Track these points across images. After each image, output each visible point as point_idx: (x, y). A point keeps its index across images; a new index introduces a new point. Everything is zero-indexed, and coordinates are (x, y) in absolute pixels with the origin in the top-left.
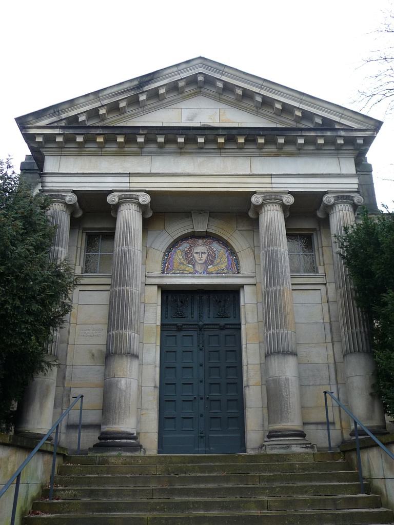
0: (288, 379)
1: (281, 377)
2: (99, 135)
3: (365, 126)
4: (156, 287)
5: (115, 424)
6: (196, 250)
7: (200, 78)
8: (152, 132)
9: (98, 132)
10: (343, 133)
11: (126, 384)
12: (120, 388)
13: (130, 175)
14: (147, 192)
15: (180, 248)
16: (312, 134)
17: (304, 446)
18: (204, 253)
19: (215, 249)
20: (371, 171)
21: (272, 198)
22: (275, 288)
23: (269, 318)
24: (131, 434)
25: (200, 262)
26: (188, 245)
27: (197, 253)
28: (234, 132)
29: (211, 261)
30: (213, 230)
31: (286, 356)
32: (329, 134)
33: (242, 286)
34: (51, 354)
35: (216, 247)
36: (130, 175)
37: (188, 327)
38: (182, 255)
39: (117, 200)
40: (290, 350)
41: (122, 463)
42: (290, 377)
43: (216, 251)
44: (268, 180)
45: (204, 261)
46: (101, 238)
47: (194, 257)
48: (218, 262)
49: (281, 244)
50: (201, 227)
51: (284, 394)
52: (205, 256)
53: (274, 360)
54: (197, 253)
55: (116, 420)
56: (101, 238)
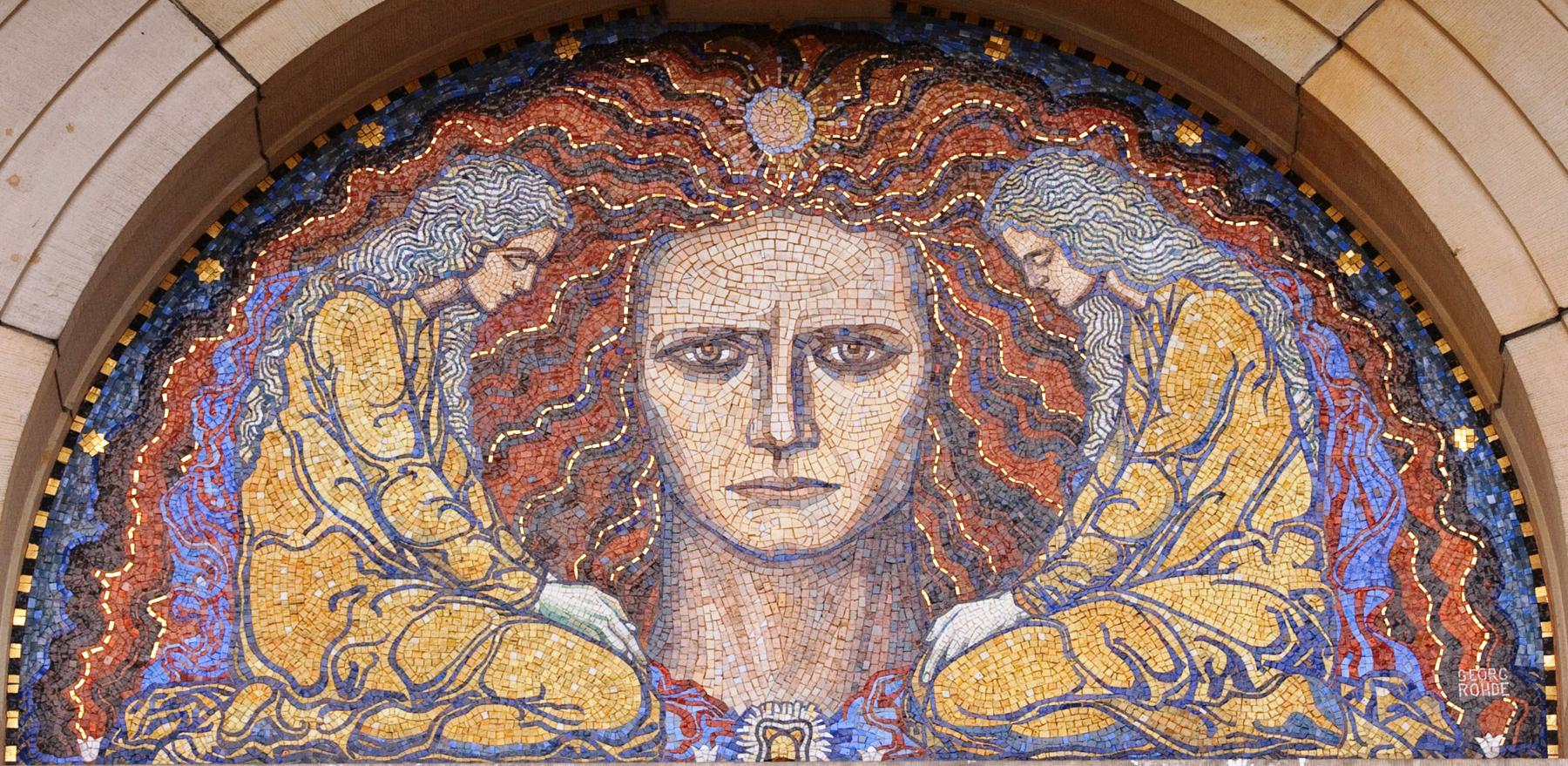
19: (1067, 281)
43: (1100, 324)
45: (846, 506)
48: (1123, 524)
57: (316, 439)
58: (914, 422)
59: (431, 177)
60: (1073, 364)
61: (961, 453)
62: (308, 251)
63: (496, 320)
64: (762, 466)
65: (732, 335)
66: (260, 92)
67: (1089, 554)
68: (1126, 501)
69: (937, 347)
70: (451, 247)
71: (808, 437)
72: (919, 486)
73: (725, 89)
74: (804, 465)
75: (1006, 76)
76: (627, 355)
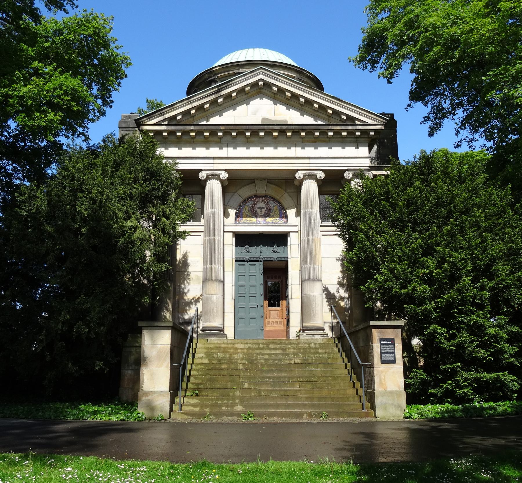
2: (192, 131)
3: (377, 122)
5: (211, 322)
6: (259, 205)
7: (261, 83)
8: (228, 128)
9: (191, 129)
10: (360, 128)
13: (214, 158)
15: (247, 204)
16: (339, 128)
17: (323, 336)
18: (264, 208)
20: (397, 126)
21: (310, 175)
23: (305, 257)
24: (220, 328)
25: (261, 214)
26: (253, 202)
27: (259, 208)
28: (284, 128)
29: (268, 214)
30: (270, 192)
31: (315, 282)
32: (350, 128)
33: (289, 232)
35: (272, 203)
36: (214, 158)
37: (253, 259)
38: (248, 210)
39: (205, 176)
40: (317, 278)
41: (73, 419)
44: (211, 161)
46: (356, 453)
47: (256, 211)
49: (315, 207)
50: (261, 191)
51: (312, 305)
52: (264, 211)
54: (259, 208)
56: (356, 453)
67: (272, 215)
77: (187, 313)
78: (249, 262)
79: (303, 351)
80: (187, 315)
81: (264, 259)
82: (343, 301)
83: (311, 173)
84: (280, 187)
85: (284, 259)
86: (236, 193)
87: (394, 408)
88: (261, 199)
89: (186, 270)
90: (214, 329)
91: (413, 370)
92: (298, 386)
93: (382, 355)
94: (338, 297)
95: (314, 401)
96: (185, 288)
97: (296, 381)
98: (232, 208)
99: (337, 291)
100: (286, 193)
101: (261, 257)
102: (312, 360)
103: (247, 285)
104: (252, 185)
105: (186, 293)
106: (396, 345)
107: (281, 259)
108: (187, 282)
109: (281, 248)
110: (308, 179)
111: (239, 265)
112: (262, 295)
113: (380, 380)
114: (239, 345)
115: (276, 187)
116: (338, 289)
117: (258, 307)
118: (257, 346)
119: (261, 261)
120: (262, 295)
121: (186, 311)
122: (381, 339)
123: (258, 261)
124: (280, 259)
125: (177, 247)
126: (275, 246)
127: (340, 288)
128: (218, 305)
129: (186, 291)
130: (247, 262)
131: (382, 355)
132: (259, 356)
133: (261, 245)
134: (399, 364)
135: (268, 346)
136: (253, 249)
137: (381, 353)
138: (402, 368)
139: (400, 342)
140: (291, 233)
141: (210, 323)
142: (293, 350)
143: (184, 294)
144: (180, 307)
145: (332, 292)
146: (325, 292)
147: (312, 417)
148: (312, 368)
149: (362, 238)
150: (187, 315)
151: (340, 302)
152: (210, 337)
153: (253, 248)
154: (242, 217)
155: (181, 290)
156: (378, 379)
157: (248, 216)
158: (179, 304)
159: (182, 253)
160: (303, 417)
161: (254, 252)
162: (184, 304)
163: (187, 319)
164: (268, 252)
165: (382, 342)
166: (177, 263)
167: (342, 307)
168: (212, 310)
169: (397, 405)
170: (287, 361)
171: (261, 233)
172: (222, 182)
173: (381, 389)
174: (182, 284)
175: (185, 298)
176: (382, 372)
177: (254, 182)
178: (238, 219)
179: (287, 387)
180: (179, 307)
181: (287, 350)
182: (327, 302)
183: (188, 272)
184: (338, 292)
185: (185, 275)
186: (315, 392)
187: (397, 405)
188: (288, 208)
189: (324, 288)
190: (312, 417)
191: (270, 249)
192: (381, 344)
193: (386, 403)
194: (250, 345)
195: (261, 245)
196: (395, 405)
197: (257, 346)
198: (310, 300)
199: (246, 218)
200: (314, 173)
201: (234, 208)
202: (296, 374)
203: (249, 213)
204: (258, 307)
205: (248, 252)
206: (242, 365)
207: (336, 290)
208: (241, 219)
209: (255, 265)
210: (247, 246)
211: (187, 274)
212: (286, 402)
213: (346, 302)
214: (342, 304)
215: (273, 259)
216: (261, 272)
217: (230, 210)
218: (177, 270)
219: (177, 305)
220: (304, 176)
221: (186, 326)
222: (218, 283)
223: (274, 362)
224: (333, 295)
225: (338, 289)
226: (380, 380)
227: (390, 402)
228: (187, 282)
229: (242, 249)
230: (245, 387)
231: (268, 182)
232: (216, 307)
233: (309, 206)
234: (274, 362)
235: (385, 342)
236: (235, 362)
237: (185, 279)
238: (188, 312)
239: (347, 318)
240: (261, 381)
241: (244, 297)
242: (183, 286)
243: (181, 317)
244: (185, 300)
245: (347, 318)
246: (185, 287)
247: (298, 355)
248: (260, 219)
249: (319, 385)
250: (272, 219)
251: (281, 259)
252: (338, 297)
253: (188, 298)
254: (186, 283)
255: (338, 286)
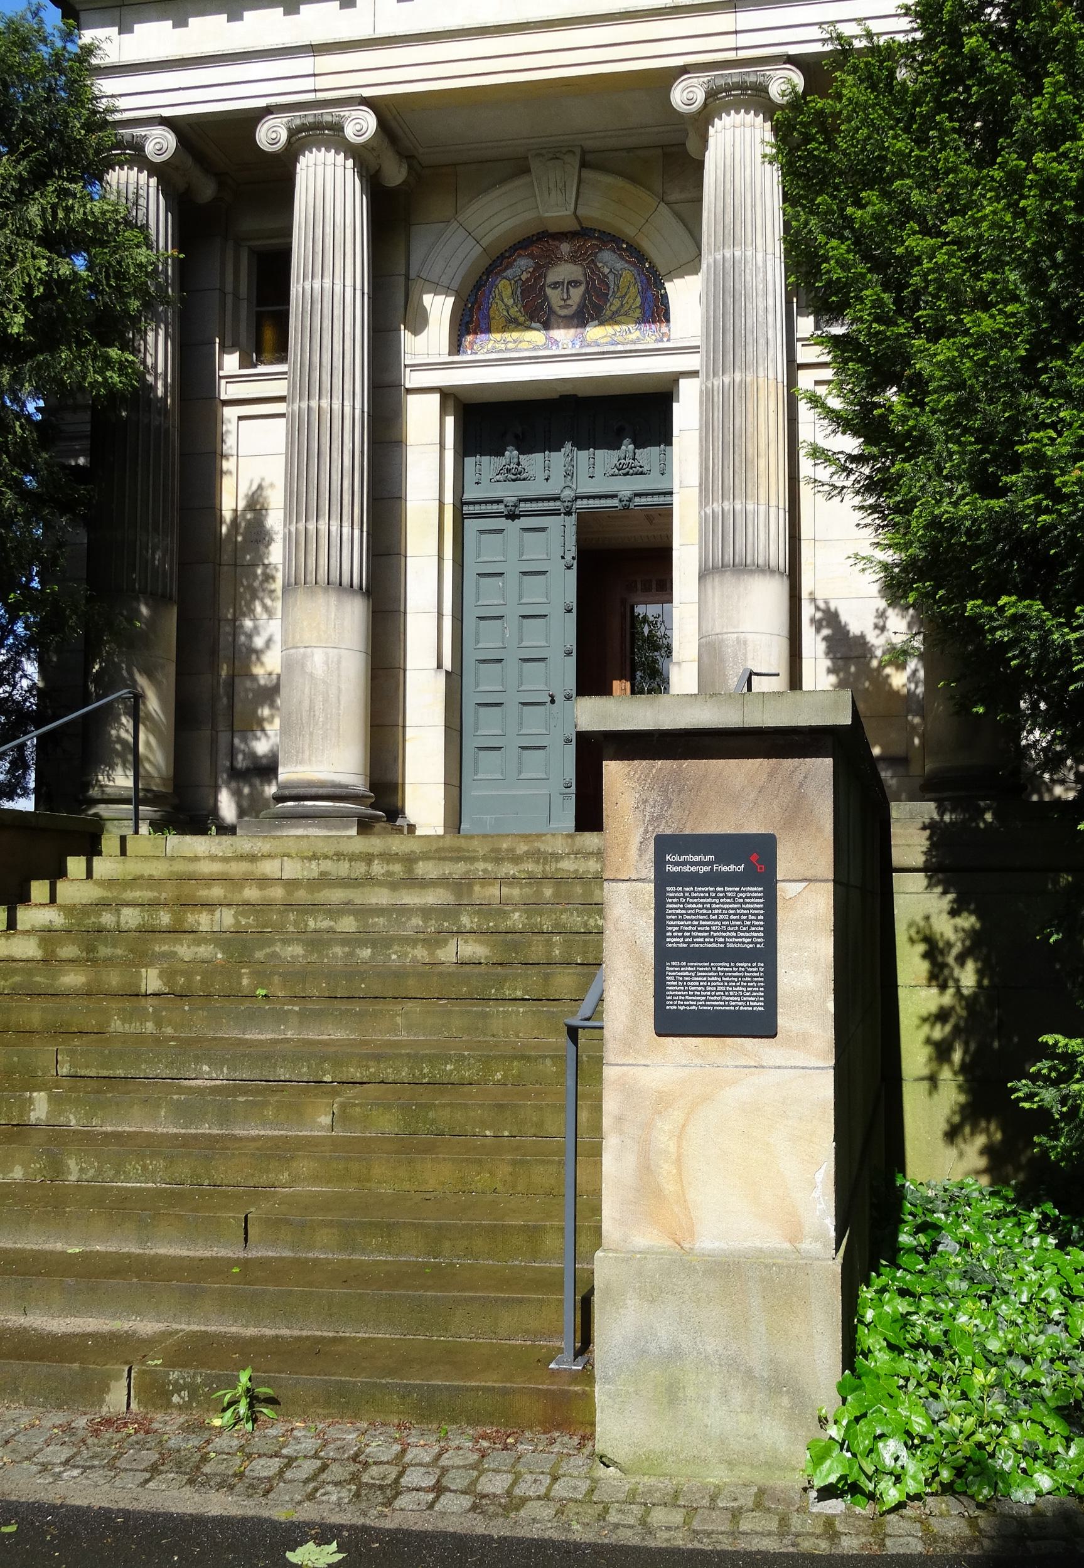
0: (745, 643)
1: (725, 636)
4: (436, 398)
5: (301, 762)
11: (326, 663)
12: (311, 675)
14: (791, 59)
18: (575, 283)
19: (606, 270)
22: (727, 380)
25: (563, 312)
26: (531, 262)
27: (556, 285)
33: (674, 378)
34: (352, 586)
35: (608, 260)
39: (700, 96)
42: (750, 637)
43: (611, 277)
44: (304, 65)
45: (574, 308)
47: (546, 298)
48: (614, 308)
52: (577, 294)
53: (713, 588)
54: (556, 285)
55: (303, 752)
57: (500, 303)
58: (584, 295)
59: (515, 260)
60: (607, 284)
61: (590, 300)
62: (499, 273)
63: (524, 283)
64: (562, 303)
65: (558, 283)
66: (835, 881)
67: (609, 313)
68: (564, 1476)
69: (588, 283)
70: (519, 272)
71: (569, 298)
72: (584, 306)
73: (557, 243)
74: (569, 302)
75: (597, 238)
76: (542, 288)
77: (263, 730)
78: (518, 517)
79: (556, 894)
80: (264, 740)
81: (580, 504)
82: (902, 667)
83: (735, 75)
84: (632, 179)
85: (656, 500)
86: (455, 224)
87: (738, 1398)
88: (565, 248)
89: (262, 561)
90: (313, 791)
91: (1049, 1039)
92: (325, 1120)
93: (673, 969)
94: (879, 653)
95: (310, 1248)
96: (256, 630)
97: (358, 1076)
98: (437, 288)
99: (876, 626)
100: (663, 208)
101: (568, 494)
102: (549, 944)
103: (512, 612)
104: (518, 182)
105: (258, 653)
106: (786, 890)
107: (649, 500)
108: (265, 607)
109: (654, 451)
110: (727, 108)
111: (482, 532)
112: (569, 654)
113: (646, 1168)
114: (276, 863)
115: (620, 182)
116: (882, 615)
117: (553, 701)
118: (360, 869)
119: (568, 513)
120: (569, 654)
121: (260, 723)
122: (665, 845)
123: (555, 513)
124: (643, 501)
125: (226, 465)
126: (627, 447)
127: (891, 612)
128: (333, 692)
129: (259, 642)
130: (512, 516)
131: (673, 969)
132: (311, 923)
133: (568, 446)
134: (803, 1040)
135: (410, 870)
136: (534, 462)
137: (664, 955)
138: (829, 1077)
139: (823, 860)
140: (682, 381)
141: (300, 768)
142: (505, 890)
143: (254, 657)
144: (238, 707)
145: (854, 629)
146: (826, 632)
147: (169, 1405)
148: (519, 994)
149: (844, 265)
150: (264, 740)
151: (889, 670)
152: (292, 826)
153: (539, 457)
154: (488, 330)
155: (243, 638)
156: (631, 1160)
157: (512, 324)
158: (231, 696)
159: (244, 490)
160: (101, 1402)
161: (541, 477)
162: (250, 695)
163: (265, 756)
164: (599, 472)
165: (675, 864)
166: (224, 529)
167: (897, 693)
168: (305, 714)
169: (761, 1370)
170: (420, 953)
171: (568, 390)
172: (358, 154)
173: (645, 1238)
174: (244, 615)
175: (258, 670)
176: (662, 1102)
177: (527, 171)
178: (469, 338)
179: (265, 1123)
180: (231, 706)
181: (477, 888)
182: (830, 671)
183: (266, 566)
184: (883, 629)
185: (255, 576)
186: (377, 1170)
187: (761, 1370)
188: (674, 273)
189: (819, 615)
190: (169, 1405)
191: (606, 458)
192: (663, 880)
193: (674, 1355)
194: (327, 866)
195: (568, 446)
196: (749, 1373)
197: (360, 869)
198: (722, 660)
199: (504, 329)
200: (751, 75)
201: (447, 292)
202: (394, 1029)
203: (514, 311)
204: (553, 701)
205: (518, 476)
206: (160, 976)
207: (871, 620)
208: (483, 337)
209: (543, 529)
210: (511, 453)
211: (264, 574)
212: (142, 1242)
213: (915, 672)
214: (898, 680)
215: (614, 502)
216: (568, 557)
217: (427, 299)
218: (226, 557)
219: (225, 700)
220: (711, 94)
221: (257, 782)
222: (333, 599)
223: (351, 954)
224: (861, 640)
225: (882, 615)
226: (646, 1168)
227: (711, 1346)
228: (265, 607)
229: (489, 464)
230: (33, 1117)
231: (584, 165)
232: (326, 700)
233: (731, 237)
234: (351, 954)
235: (697, 863)
236: (164, 955)
237: (254, 596)
238: (267, 727)
239: (917, 741)
240: (167, 1073)
241: (500, 661)
242: (248, 624)
243: (242, 746)
244: (254, 678)
245: (917, 741)
246: (256, 628)
247: (505, 915)
248: (559, 334)
249: (446, 1113)
250: (609, 330)
251: (649, 500)
252: (879, 653)
253: (269, 668)
254: (259, 608)
255: (882, 604)
